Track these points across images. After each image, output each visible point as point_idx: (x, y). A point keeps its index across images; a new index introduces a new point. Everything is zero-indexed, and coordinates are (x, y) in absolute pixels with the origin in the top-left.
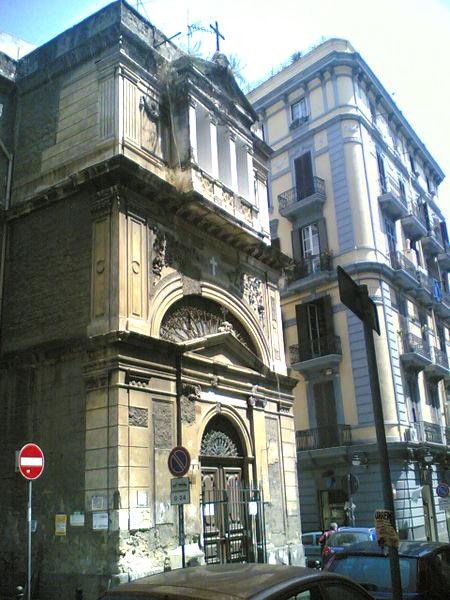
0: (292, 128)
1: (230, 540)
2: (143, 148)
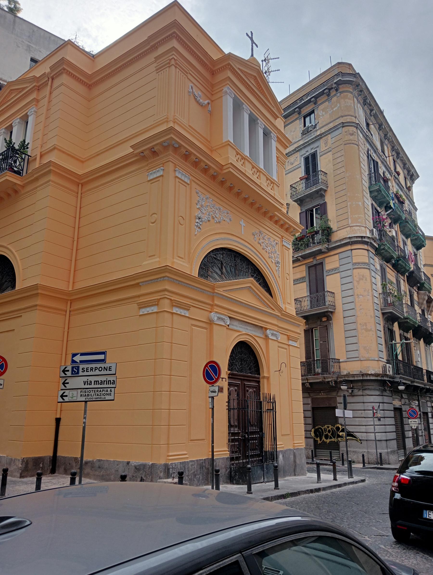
0: (303, 133)
1: (249, 440)
2: (189, 126)
